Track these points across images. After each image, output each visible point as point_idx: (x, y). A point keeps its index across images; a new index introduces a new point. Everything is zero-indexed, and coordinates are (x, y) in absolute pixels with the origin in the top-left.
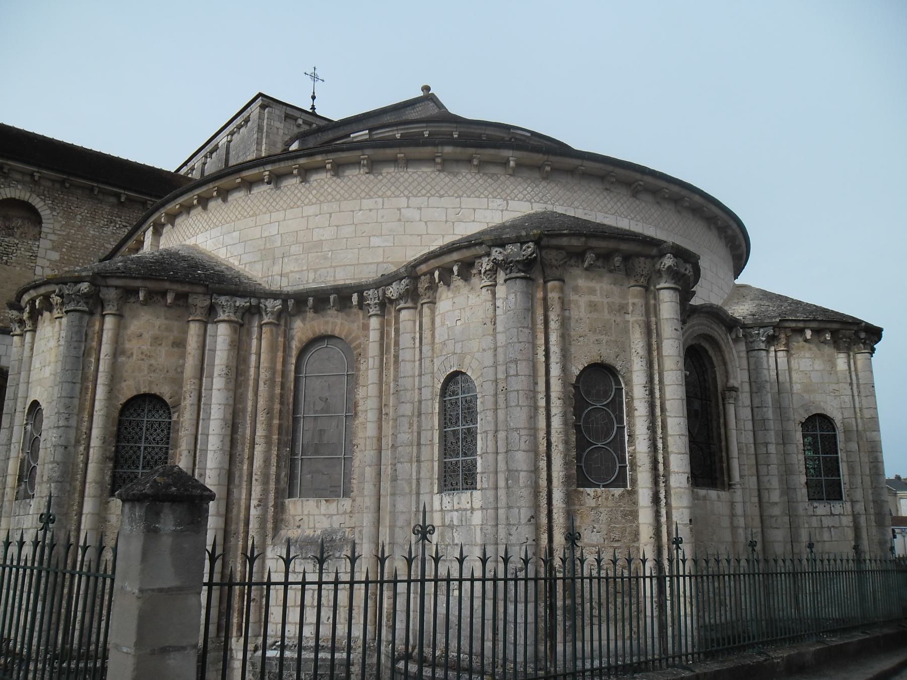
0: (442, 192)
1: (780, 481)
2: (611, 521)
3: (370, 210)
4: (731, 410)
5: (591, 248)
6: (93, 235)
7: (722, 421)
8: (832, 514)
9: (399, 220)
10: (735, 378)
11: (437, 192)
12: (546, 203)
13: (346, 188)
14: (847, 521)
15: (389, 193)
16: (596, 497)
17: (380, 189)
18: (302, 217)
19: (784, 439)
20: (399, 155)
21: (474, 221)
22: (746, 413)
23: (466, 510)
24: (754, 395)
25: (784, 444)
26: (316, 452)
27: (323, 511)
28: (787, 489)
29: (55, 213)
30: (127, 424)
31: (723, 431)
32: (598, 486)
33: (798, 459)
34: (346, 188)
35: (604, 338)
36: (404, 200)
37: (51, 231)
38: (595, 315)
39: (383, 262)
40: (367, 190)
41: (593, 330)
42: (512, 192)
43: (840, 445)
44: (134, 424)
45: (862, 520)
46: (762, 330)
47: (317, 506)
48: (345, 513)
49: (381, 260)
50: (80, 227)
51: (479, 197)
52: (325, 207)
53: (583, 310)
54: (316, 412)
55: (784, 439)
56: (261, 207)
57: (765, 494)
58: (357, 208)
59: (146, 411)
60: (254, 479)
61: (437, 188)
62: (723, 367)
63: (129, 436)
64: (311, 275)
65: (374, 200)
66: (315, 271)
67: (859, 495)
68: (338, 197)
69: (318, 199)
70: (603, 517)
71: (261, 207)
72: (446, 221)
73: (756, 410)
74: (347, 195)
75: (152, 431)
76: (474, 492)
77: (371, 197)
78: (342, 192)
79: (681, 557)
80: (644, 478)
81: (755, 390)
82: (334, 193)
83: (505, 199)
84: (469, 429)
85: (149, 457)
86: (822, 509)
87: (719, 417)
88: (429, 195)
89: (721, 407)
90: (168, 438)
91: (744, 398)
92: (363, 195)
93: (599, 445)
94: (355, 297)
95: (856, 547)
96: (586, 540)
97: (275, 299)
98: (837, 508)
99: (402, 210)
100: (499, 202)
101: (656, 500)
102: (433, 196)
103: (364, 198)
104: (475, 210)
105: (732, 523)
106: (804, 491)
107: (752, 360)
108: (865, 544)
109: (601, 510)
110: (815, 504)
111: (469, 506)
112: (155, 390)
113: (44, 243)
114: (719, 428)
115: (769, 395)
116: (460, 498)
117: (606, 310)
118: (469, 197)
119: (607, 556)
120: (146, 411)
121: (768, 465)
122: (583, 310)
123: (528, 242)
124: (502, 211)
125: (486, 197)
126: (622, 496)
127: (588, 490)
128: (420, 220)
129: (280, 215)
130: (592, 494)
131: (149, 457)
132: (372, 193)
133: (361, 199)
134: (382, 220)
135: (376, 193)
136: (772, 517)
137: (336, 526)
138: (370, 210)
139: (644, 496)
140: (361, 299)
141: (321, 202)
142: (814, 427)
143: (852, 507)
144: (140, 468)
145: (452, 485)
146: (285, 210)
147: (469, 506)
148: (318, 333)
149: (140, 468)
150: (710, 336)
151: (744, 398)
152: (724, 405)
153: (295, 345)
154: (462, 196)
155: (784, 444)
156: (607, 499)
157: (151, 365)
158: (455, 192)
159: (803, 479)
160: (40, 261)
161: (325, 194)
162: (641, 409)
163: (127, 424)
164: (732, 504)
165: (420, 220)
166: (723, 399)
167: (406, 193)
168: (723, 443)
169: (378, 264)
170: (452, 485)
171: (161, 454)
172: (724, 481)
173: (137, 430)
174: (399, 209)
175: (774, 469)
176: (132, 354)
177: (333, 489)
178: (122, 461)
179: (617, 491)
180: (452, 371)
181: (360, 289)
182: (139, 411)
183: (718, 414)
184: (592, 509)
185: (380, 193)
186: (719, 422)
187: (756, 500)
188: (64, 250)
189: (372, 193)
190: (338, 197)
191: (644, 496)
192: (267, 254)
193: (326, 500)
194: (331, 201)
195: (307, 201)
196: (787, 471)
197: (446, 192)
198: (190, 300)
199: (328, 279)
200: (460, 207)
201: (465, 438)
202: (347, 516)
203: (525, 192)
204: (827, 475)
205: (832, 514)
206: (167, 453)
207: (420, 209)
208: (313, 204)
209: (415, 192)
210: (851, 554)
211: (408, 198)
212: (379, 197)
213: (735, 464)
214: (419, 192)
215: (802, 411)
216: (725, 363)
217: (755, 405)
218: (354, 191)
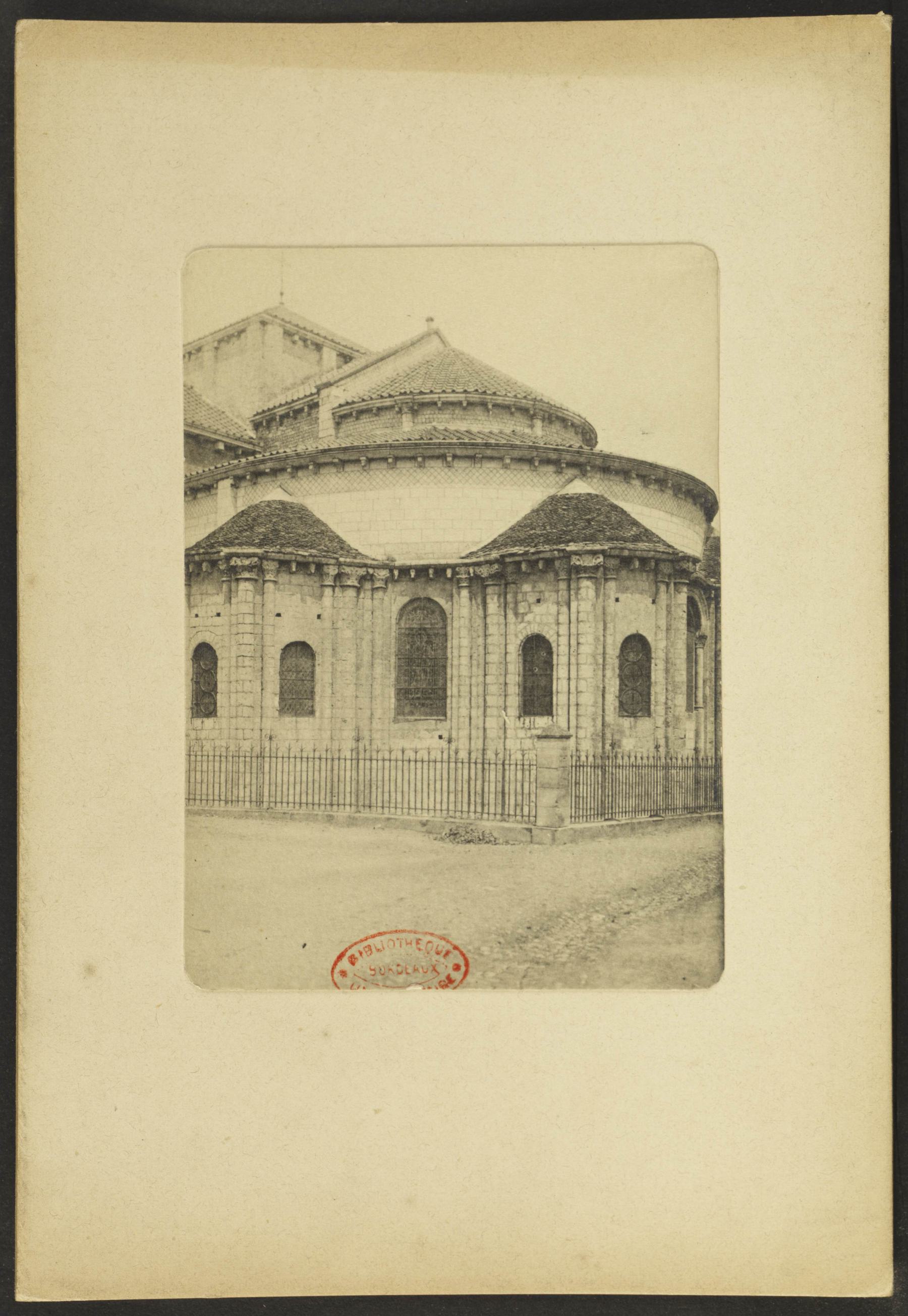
94: (449, 573)
140: (455, 573)
181: (453, 567)
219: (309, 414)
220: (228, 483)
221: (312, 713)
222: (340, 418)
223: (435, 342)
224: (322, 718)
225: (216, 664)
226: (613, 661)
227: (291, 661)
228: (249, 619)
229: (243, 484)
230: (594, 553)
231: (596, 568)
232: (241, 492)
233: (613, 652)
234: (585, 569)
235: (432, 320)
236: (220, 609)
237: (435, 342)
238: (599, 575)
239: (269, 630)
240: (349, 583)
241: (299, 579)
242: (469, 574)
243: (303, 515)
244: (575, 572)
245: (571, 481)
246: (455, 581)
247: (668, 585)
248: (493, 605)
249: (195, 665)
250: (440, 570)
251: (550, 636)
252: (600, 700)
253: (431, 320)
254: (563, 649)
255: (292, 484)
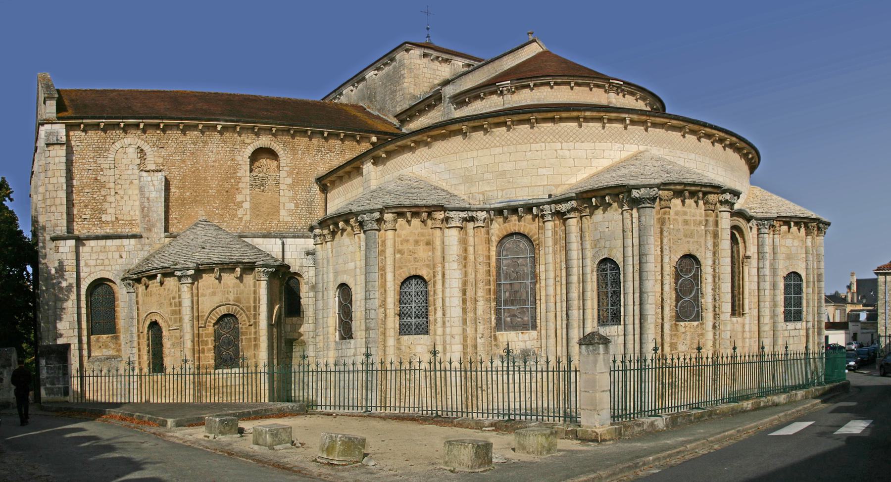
0: (583, 139)
1: (770, 311)
2: (692, 339)
3: (537, 151)
4: (746, 269)
5: (687, 190)
6: (310, 163)
7: (741, 276)
8: (795, 329)
9: (557, 158)
10: (750, 251)
11: (580, 139)
12: (647, 145)
13: (520, 136)
14: (803, 333)
15: (549, 140)
16: (685, 327)
17: (543, 137)
18: (491, 155)
19: (774, 286)
20: (556, 117)
21: (603, 158)
22: (754, 271)
23: (614, 336)
24: (760, 261)
25: (774, 289)
26: (512, 304)
27: (520, 339)
28: (774, 316)
29: (286, 153)
30: (403, 294)
31: (741, 282)
32: (686, 321)
33: (781, 298)
34: (520, 136)
35: (691, 240)
36: (560, 144)
37: (285, 165)
38: (687, 227)
39: (547, 185)
40: (534, 138)
41: (686, 236)
42: (626, 138)
43: (804, 290)
44: (407, 293)
45: (811, 331)
46: (766, 222)
47: (516, 336)
48: (534, 339)
49: (546, 183)
50: (302, 159)
51: (606, 142)
52: (506, 149)
53: (680, 224)
54: (511, 280)
55: (774, 286)
56: (459, 148)
57: (762, 319)
58: (528, 150)
59: (413, 285)
60: (478, 322)
61: (580, 136)
62: (743, 244)
63: (405, 301)
64: (500, 194)
65: (539, 144)
66: (502, 190)
67: (810, 318)
68: (515, 142)
69: (500, 144)
70: (688, 337)
71: (459, 148)
72: (586, 158)
73: (760, 270)
74: (521, 141)
75: (417, 297)
76: (619, 326)
77: (537, 143)
78: (517, 139)
79: (700, 356)
80: (709, 316)
81: (760, 257)
82: (512, 139)
83: (622, 144)
84: (614, 291)
85: (417, 312)
86: (791, 325)
87: (739, 274)
88: (575, 141)
89: (741, 268)
90: (427, 300)
91: (754, 262)
92: (531, 141)
93: (687, 299)
95: (806, 347)
96: (679, 349)
97: (482, 211)
98: (798, 325)
99: (558, 151)
100: (618, 145)
101: (714, 327)
102: (577, 141)
103: (532, 143)
104: (604, 150)
105: (743, 336)
106: (782, 316)
107: (760, 239)
108: (811, 346)
109: (688, 333)
110: (787, 324)
111: (616, 334)
112: (419, 273)
113: (283, 174)
114: (739, 280)
115: (768, 261)
116: (216, 317)
117: (692, 224)
118: (600, 142)
119: (688, 357)
120: (413, 285)
121: (764, 302)
122: (680, 224)
123: (653, 188)
124: (621, 151)
125: (611, 142)
126: (698, 325)
127: (682, 324)
128: (570, 158)
129: (475, 154)
130: (683, 326)
131: (417, 312)
132: (537, 140)
133: (531, 143)
134: (545, 158)
135: (540, 140)
136: (764, 331)
137: (529, 347)
138: (537, 151)
139: (709, 324)
141: (503, 146)
142: (791, 279)
143: (806, 324)
144: (413, 318)
145: (603, 322)
146: (478, 150)
147: (616, 334)
148: (509, 232)
149: (413, 318)
150: (738, 226)
151: (754, 262)
152: (743, 267)
153: (495, 239)
154: (596, 142)
155: (774, 289)
156: (690, 328)
157: (416, 258)
158: (592, 139)
159: (782, 309)
160: (282, 187)
161: (506, 140)
162: (710, 279)
163: (403, 294)
164: (743, 325)
165: (570, 158)
166: (742, 263)
167: (560, 140)
168: (741, 290)
169: (544, 186)
170: (603, 322)
171: (423, 310)
172: (740, 312)
173: (409, 297)
174: (556, 150)
175: (767, 305)
176: (404, 252)
177: (525, 326)
178: (403, 315)
179: (695, 323)
180: (604, 257)
181: (538, 205)
182: (410, 286)
183: (739, 272)
184: (683, 333)
185: (543, 140)
186: (739, 277)
187: (757, 322)
188: (294, 176)
189: (537, 140)
190: (515, 142)
191: (709, 324)
192: (468, 180)
193: (522, 333)
194: (510, 145)
195: (493, 144)
196: (775, 305)
197: (586, 139)
198: (433, 216)
199: (512, 196)
200: (595, 149)
201: (612, 296)
202: (535, 341)
203: (634, 139)
204: (794, 307)
205: (795, 329)
206: (427, 309)
207: (569, 150)
208: (497, 147)
209: (566, 139)
210: (804, 351)
211: (562, 143)
212: (543, 142)
213: (746, 302)
214: (569, 139)
215: (784, 270)
216: (744, 242)
217: (760, 267)
218: (525, 138)
221: (427, 333)
224: (435, 334)
242: (551, 210)
250: (528, 208)
252: (660, 311)
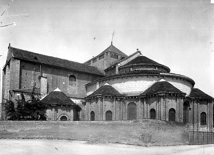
181: (138, 96)
219: (114, 69)
220: (98, 82)
222: (119, 69)
223: (139, 54)
225: (94, 115)
226: (168, 114)
227: (108, 114)
228: (100, 107)
229: (101, 82)
230: (163, 93)
231: (163, 96)
232: (101, 84)
233: (168, 112)
234: (162, 96)
235: (138, 49)
236: (95, 105)
237: (139, 54)
238: (164, 97)
239: (104, 109)
240: (118, 100)
241: (109, 100)
243: (113, 89)
244: (160, 97)
245: (161, 79)
246: (138, 99)
247: (179, 99)
248: (145, 103)
249: (22, 120)
250: (135, 97)
251: (155, 109)
253: (138, 49)
254: (114, 113)
255: (109, 82)
